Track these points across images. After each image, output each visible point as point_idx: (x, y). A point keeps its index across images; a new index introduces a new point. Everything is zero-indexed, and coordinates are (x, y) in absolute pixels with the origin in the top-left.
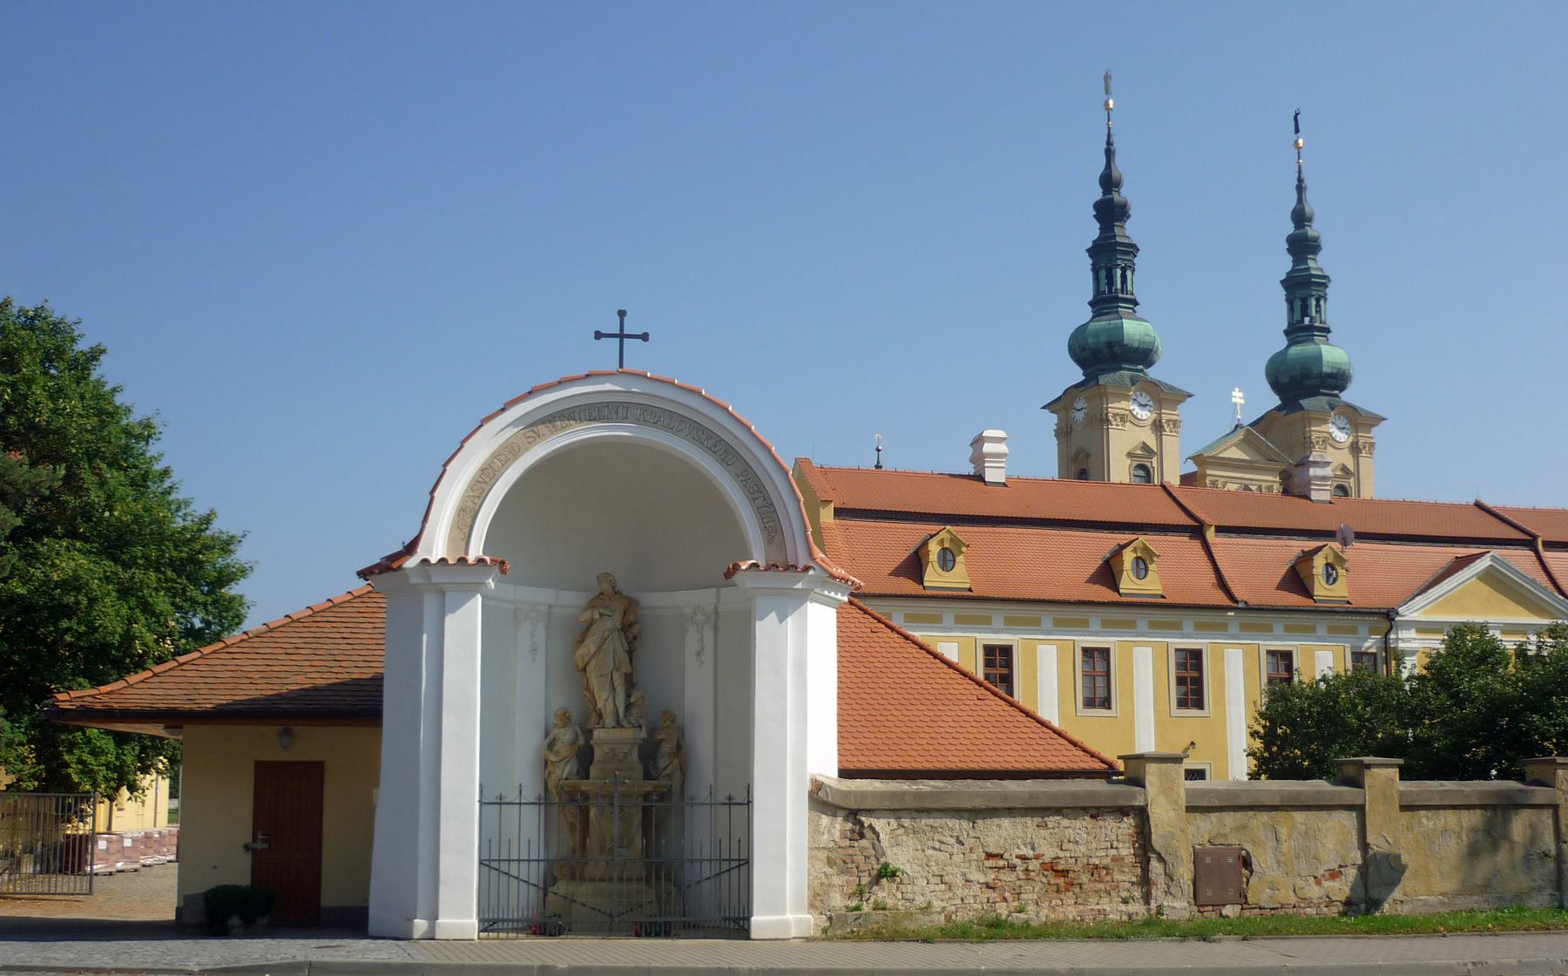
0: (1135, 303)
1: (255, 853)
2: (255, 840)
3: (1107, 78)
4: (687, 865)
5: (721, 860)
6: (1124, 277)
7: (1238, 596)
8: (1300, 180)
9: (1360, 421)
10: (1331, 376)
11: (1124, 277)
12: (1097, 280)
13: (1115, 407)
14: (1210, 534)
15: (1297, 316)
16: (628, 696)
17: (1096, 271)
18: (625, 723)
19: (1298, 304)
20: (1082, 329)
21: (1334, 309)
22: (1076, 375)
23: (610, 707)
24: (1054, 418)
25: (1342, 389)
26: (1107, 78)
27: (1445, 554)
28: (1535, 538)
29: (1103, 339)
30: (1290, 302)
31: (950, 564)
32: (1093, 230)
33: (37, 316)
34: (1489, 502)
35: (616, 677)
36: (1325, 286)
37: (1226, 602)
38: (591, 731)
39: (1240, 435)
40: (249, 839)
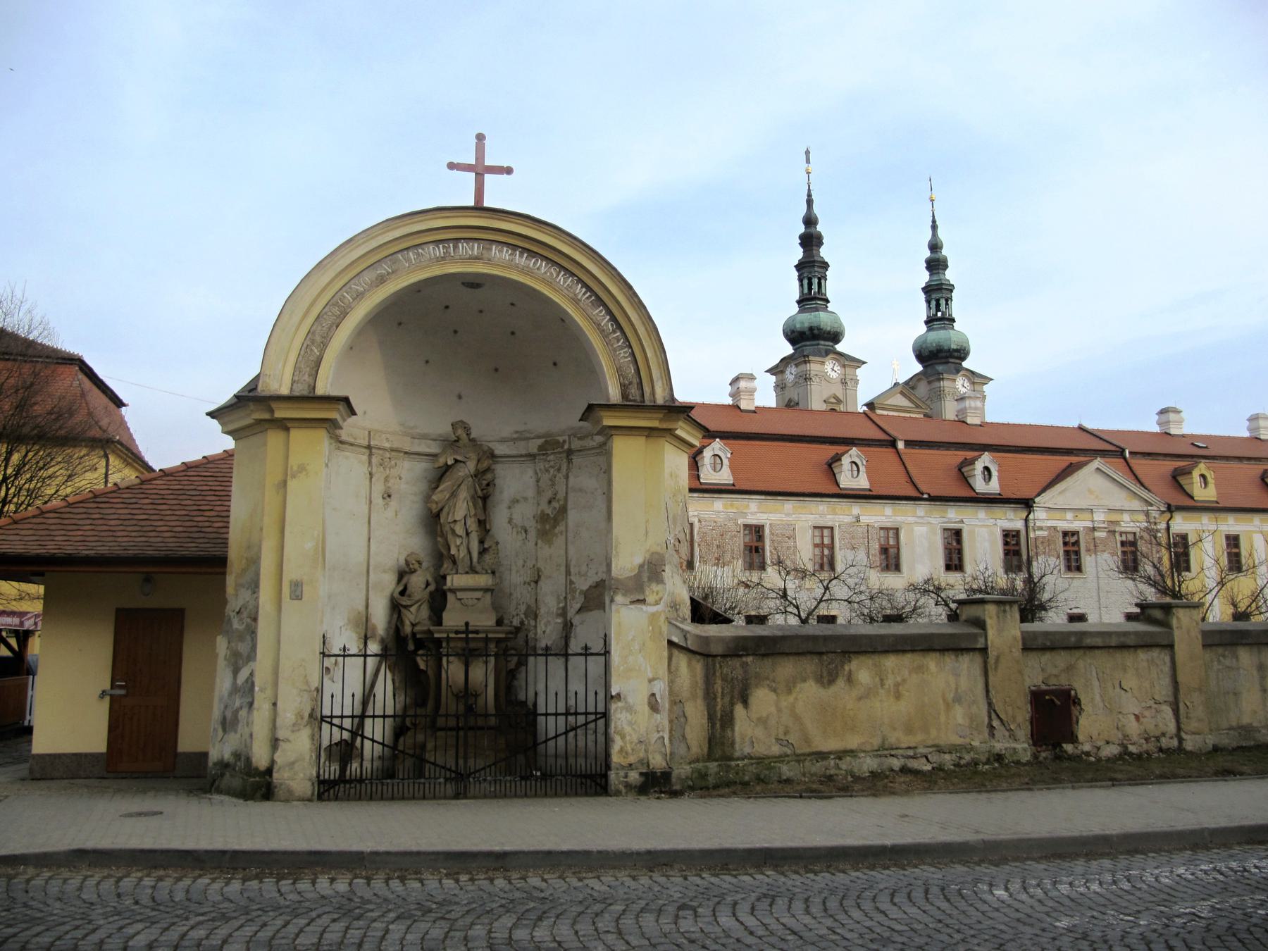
0: (828, 301)
1: (113, 700)
2: (113, 687)
3: (807, 153)
4: (541, 719)
5: (586, 714)
6: (820, 284)
7: (923, 489)
8: (934, 221)
9: (978, 380)
10: (957, 351)
11: (820, 284)
12: (802, 285)
13: (813, 367)
14: (901, 445)
15: (933, 311)
16: (481, 542)
17: (801, 280)
18: (478, 568)
19: (933, 303)
20: (792, 319)
21: (958, 307)
22: (788, 349)
23: (463, 553)
24: (773, 378)
25: (964, 359)
26: (807, 153)
27: (1065, 460)
28: (1123, 450)
29: (807, 325)
30: (928, 302)
31: (718, 467)
32: (799, 253)
33: (467, 631)
34: (1089, 425)
35: (469, 522)
36: (951, 291)
37: (914, 493)
38: (444, 577)
39: (899, 389)
40: (107, 686)
